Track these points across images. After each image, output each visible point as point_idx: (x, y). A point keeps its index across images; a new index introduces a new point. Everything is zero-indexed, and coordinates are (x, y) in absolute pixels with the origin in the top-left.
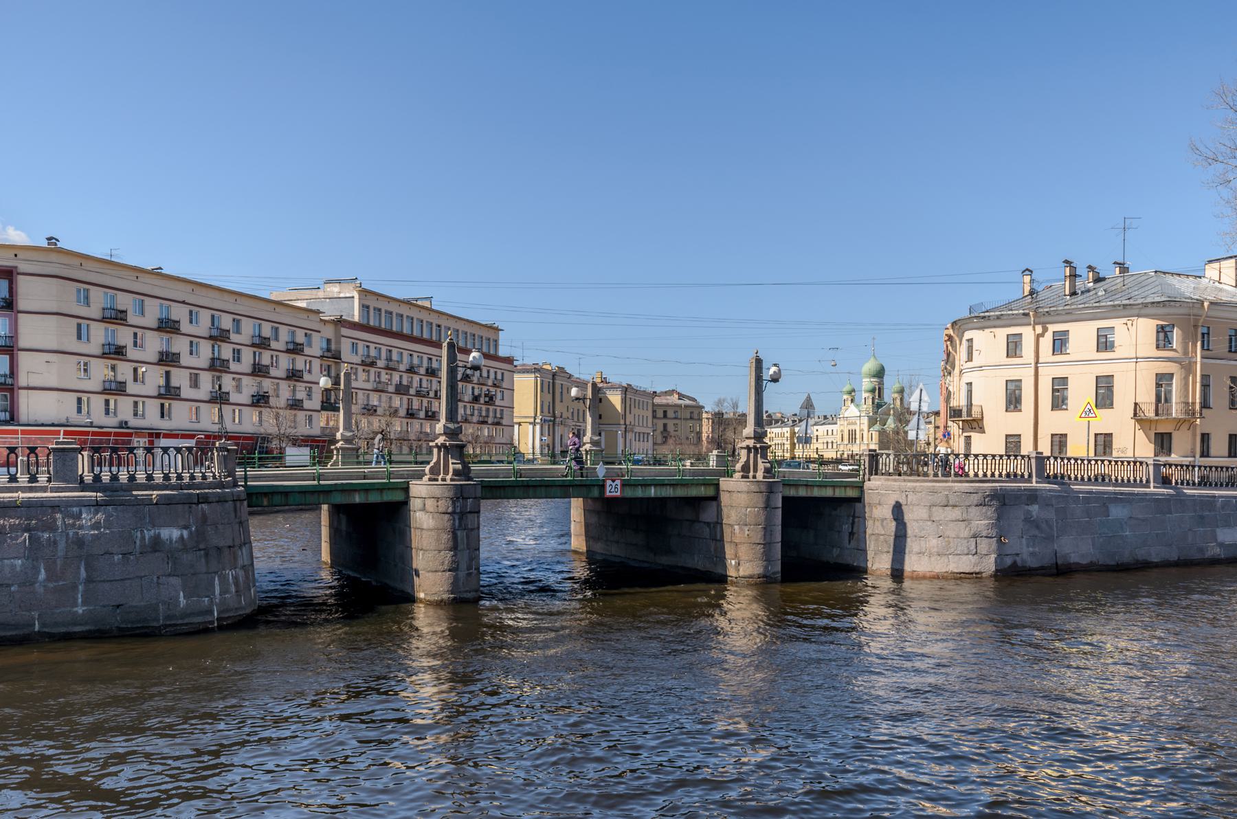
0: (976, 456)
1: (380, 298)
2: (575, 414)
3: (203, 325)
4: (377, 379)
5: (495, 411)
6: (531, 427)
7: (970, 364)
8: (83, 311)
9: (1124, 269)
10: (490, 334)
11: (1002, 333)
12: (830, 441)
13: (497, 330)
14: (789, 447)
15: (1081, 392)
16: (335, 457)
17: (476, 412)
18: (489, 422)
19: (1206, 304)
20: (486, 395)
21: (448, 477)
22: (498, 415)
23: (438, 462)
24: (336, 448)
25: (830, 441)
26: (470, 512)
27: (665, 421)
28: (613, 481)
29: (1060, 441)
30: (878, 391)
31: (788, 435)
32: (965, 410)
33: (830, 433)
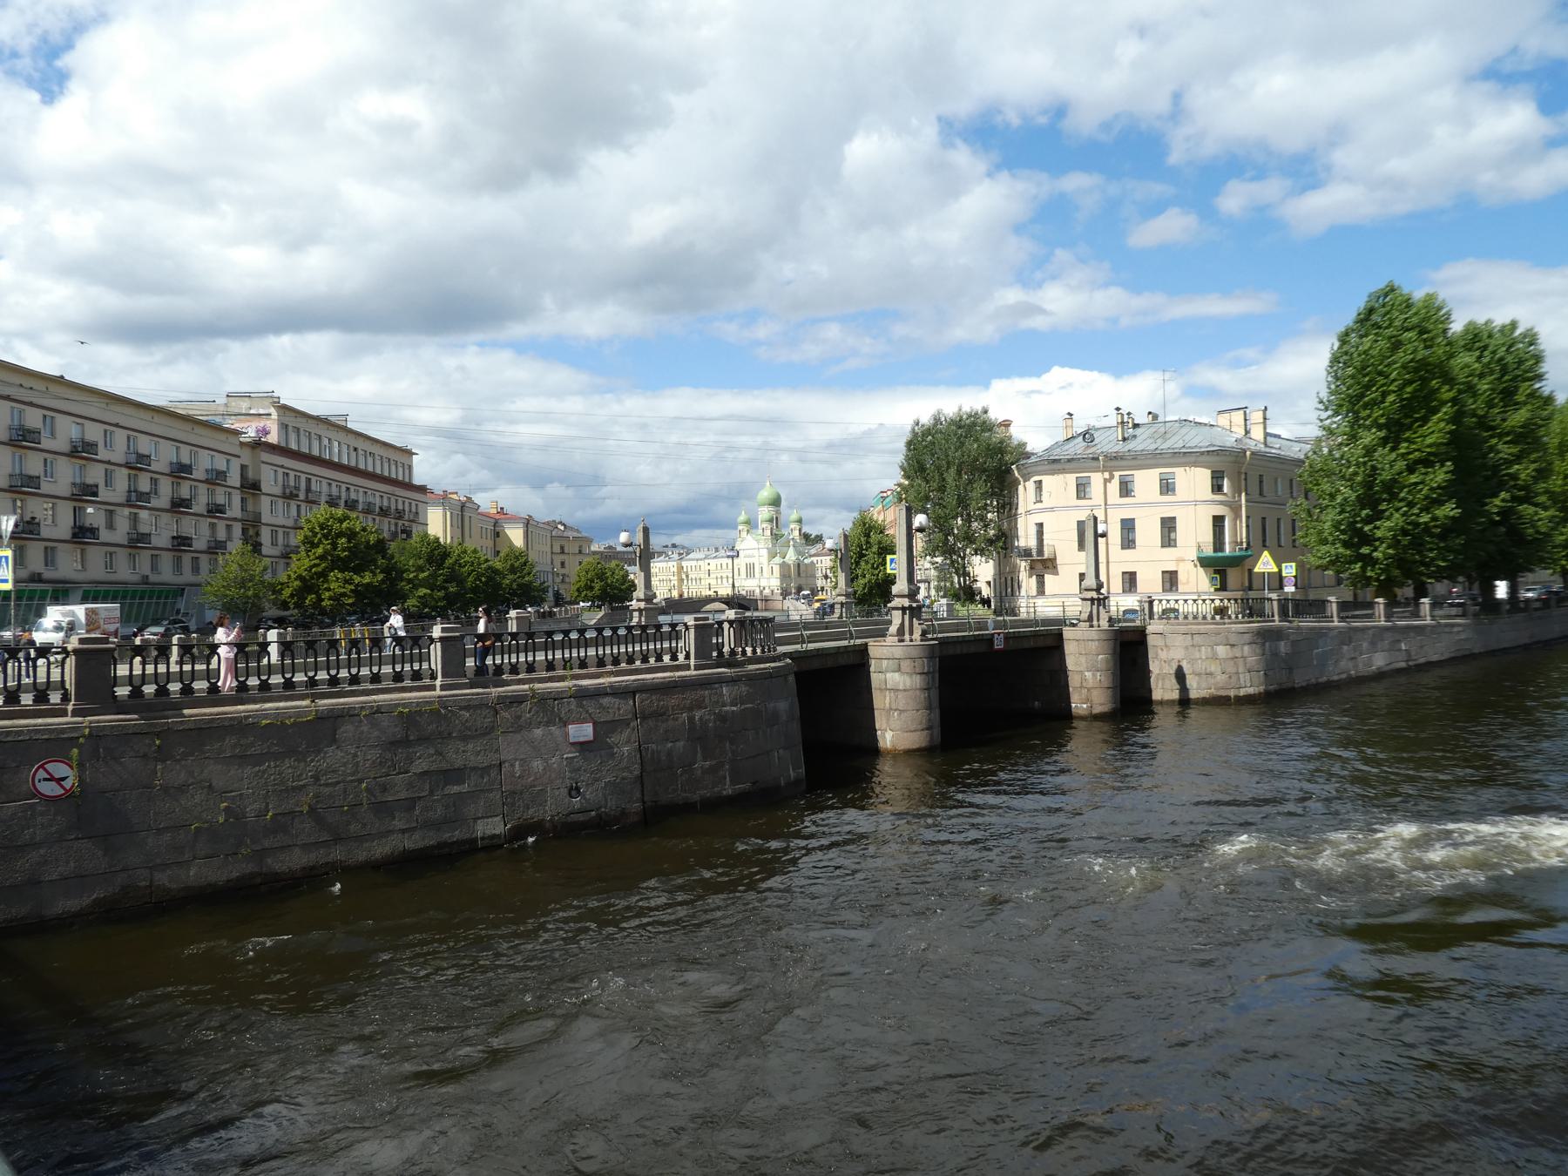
7: (1039, 505)
11: (1071, 479)
12: (724, 576)
13: (410, 453)
14: (676, 583)
15: (1149, 532)
19: (1248, 453)
20: (403, 531)
25: (724, 576)
27: (562, 557)
30: (775, 521)
31: (675, 569)
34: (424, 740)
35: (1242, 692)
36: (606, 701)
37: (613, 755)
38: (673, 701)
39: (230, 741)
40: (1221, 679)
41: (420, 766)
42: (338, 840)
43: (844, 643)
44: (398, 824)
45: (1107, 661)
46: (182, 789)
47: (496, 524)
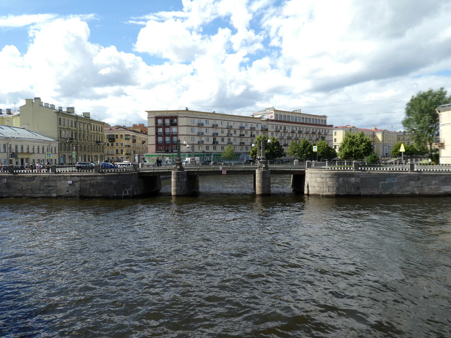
3: (260, 128)
8: (193, 125)
34: (46, 181)
35: (324, 194)
36: (75, 177)
37: (75, 187)
38: (87, 178)
39: (22, 178)
40: (317, 189)
41: (45, 184)
42: (33, 193)
43: (149, 171)
44: (41, 192)
45: (260, 180)
46: (17, 184)
47: (374, 133)
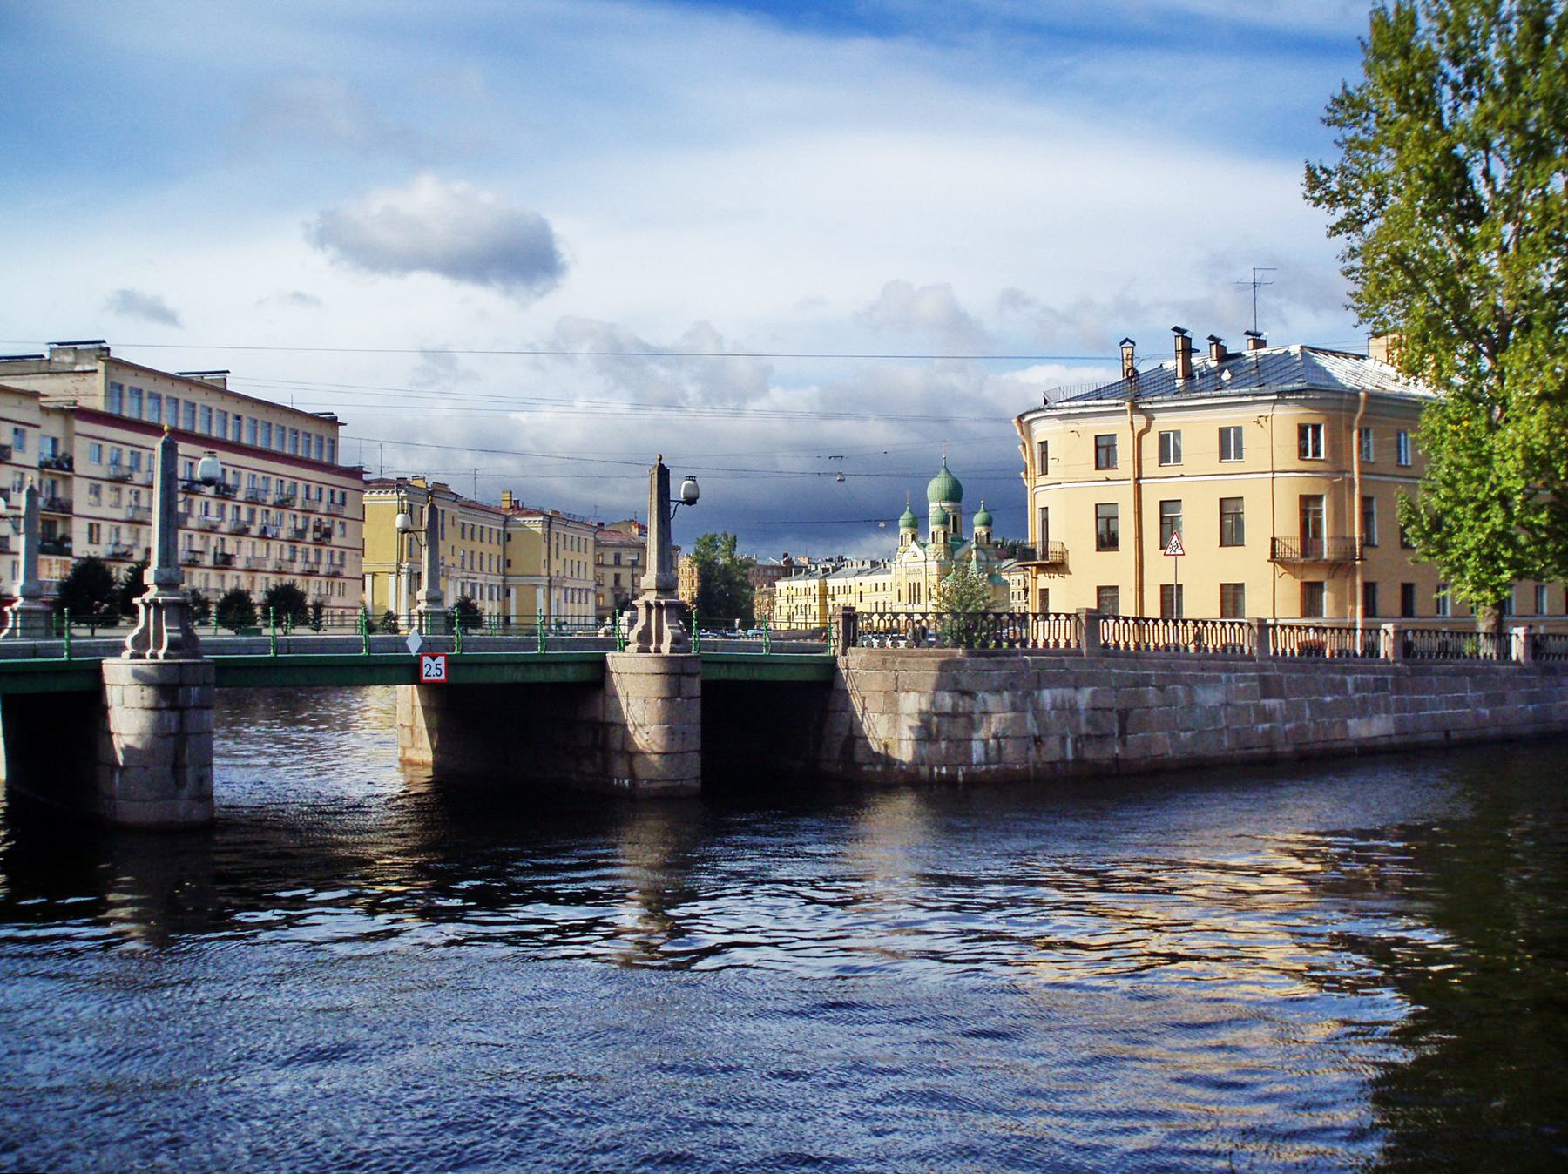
0: (1057, 615)
1: (141, 374)
2: (468, 560)
4: (134, 503)
5: (332, 554)
6: (392, 579)
9: (1259, 343)
10: (325, 431)
15: (1200, 523)
16: (10, 624)
17: (299, 556)
18: (322, 572)
21: (161, 653)
22: (337, 561)
23: (145, 630)
24: (12, 610)
26: (196, 707)
27: (618, 570)
28: (434, 658)
29: (1171, 596)
32: (1039, 549)
33: (880, 587)
